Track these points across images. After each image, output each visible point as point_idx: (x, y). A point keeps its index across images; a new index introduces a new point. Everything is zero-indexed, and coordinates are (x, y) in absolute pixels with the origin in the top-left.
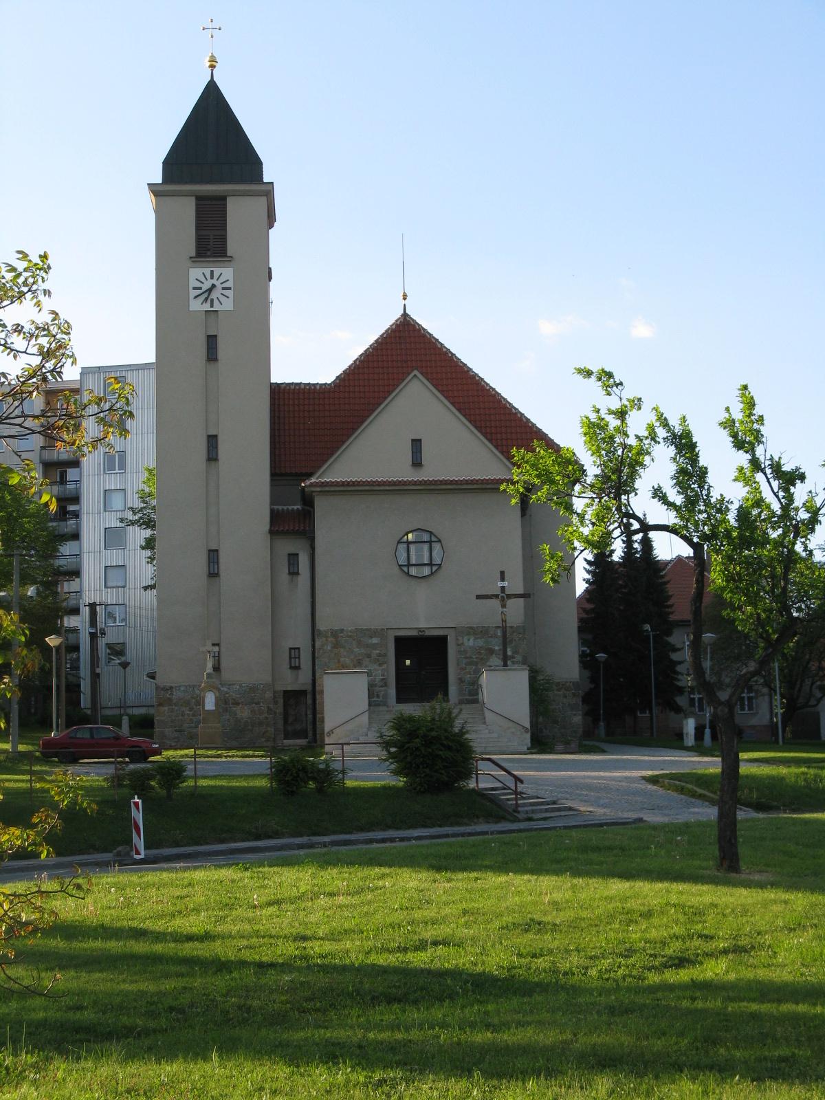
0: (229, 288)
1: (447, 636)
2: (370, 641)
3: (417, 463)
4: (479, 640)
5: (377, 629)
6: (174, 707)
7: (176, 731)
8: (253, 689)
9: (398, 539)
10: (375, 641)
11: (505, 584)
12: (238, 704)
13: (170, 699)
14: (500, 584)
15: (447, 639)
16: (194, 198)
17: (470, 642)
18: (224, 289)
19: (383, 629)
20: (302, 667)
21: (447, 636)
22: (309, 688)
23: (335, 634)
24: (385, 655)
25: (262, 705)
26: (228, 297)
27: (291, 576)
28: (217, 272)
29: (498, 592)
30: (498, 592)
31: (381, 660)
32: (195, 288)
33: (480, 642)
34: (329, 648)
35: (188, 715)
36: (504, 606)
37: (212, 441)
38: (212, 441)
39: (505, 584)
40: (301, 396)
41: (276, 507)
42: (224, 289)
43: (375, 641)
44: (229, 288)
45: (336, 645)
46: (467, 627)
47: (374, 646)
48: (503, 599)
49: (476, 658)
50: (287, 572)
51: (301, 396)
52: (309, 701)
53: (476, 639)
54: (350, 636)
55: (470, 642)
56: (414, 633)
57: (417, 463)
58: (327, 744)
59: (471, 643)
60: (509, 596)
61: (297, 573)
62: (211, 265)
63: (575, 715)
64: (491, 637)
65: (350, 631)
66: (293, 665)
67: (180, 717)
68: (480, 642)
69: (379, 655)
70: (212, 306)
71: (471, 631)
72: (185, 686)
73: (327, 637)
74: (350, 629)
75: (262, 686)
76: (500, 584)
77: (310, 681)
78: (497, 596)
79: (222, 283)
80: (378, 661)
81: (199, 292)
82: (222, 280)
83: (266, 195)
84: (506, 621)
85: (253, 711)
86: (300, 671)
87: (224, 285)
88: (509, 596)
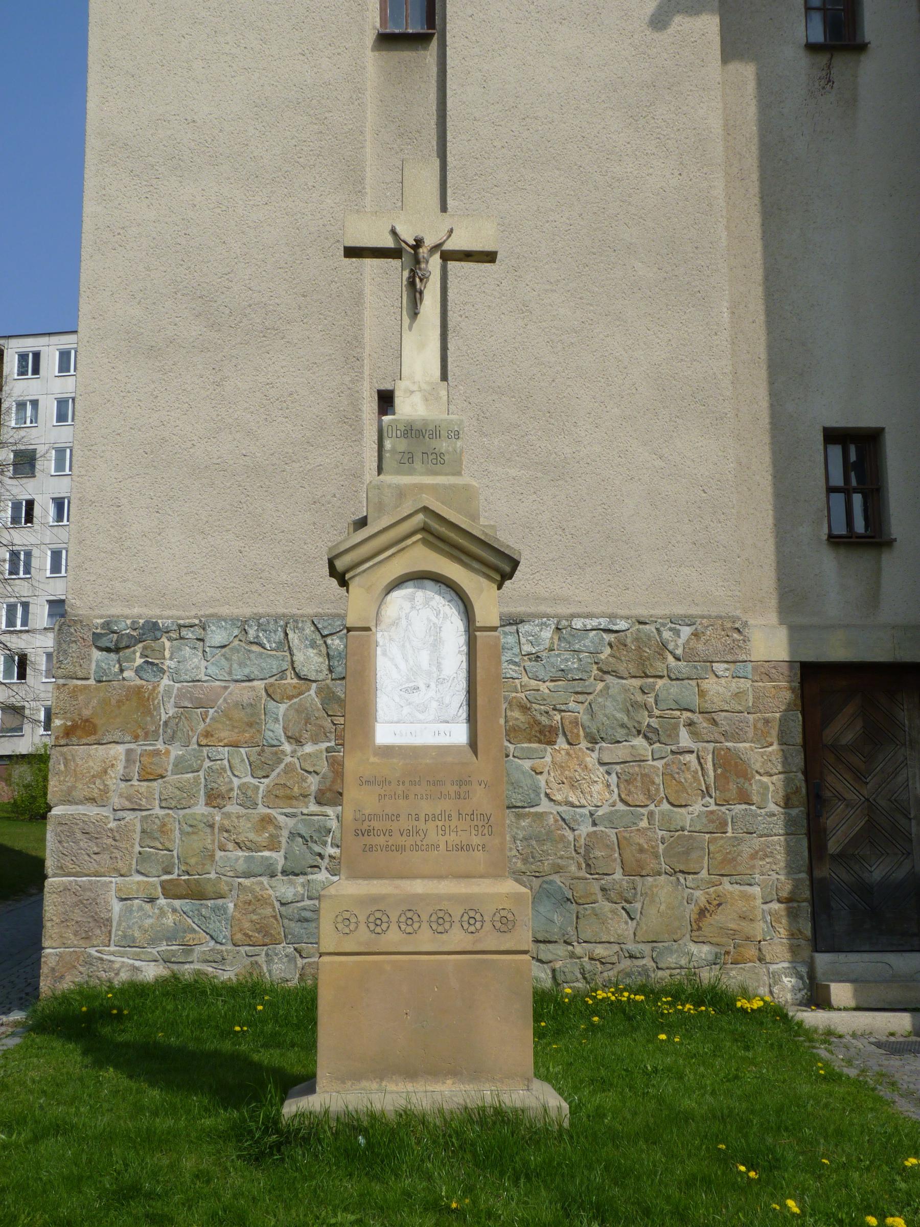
7: (170, 890)
27: (823, 59)
66: (840, 529)
67: (200, 809)
72: (233, 620)
75: (686, 631)
86: (888, 559)
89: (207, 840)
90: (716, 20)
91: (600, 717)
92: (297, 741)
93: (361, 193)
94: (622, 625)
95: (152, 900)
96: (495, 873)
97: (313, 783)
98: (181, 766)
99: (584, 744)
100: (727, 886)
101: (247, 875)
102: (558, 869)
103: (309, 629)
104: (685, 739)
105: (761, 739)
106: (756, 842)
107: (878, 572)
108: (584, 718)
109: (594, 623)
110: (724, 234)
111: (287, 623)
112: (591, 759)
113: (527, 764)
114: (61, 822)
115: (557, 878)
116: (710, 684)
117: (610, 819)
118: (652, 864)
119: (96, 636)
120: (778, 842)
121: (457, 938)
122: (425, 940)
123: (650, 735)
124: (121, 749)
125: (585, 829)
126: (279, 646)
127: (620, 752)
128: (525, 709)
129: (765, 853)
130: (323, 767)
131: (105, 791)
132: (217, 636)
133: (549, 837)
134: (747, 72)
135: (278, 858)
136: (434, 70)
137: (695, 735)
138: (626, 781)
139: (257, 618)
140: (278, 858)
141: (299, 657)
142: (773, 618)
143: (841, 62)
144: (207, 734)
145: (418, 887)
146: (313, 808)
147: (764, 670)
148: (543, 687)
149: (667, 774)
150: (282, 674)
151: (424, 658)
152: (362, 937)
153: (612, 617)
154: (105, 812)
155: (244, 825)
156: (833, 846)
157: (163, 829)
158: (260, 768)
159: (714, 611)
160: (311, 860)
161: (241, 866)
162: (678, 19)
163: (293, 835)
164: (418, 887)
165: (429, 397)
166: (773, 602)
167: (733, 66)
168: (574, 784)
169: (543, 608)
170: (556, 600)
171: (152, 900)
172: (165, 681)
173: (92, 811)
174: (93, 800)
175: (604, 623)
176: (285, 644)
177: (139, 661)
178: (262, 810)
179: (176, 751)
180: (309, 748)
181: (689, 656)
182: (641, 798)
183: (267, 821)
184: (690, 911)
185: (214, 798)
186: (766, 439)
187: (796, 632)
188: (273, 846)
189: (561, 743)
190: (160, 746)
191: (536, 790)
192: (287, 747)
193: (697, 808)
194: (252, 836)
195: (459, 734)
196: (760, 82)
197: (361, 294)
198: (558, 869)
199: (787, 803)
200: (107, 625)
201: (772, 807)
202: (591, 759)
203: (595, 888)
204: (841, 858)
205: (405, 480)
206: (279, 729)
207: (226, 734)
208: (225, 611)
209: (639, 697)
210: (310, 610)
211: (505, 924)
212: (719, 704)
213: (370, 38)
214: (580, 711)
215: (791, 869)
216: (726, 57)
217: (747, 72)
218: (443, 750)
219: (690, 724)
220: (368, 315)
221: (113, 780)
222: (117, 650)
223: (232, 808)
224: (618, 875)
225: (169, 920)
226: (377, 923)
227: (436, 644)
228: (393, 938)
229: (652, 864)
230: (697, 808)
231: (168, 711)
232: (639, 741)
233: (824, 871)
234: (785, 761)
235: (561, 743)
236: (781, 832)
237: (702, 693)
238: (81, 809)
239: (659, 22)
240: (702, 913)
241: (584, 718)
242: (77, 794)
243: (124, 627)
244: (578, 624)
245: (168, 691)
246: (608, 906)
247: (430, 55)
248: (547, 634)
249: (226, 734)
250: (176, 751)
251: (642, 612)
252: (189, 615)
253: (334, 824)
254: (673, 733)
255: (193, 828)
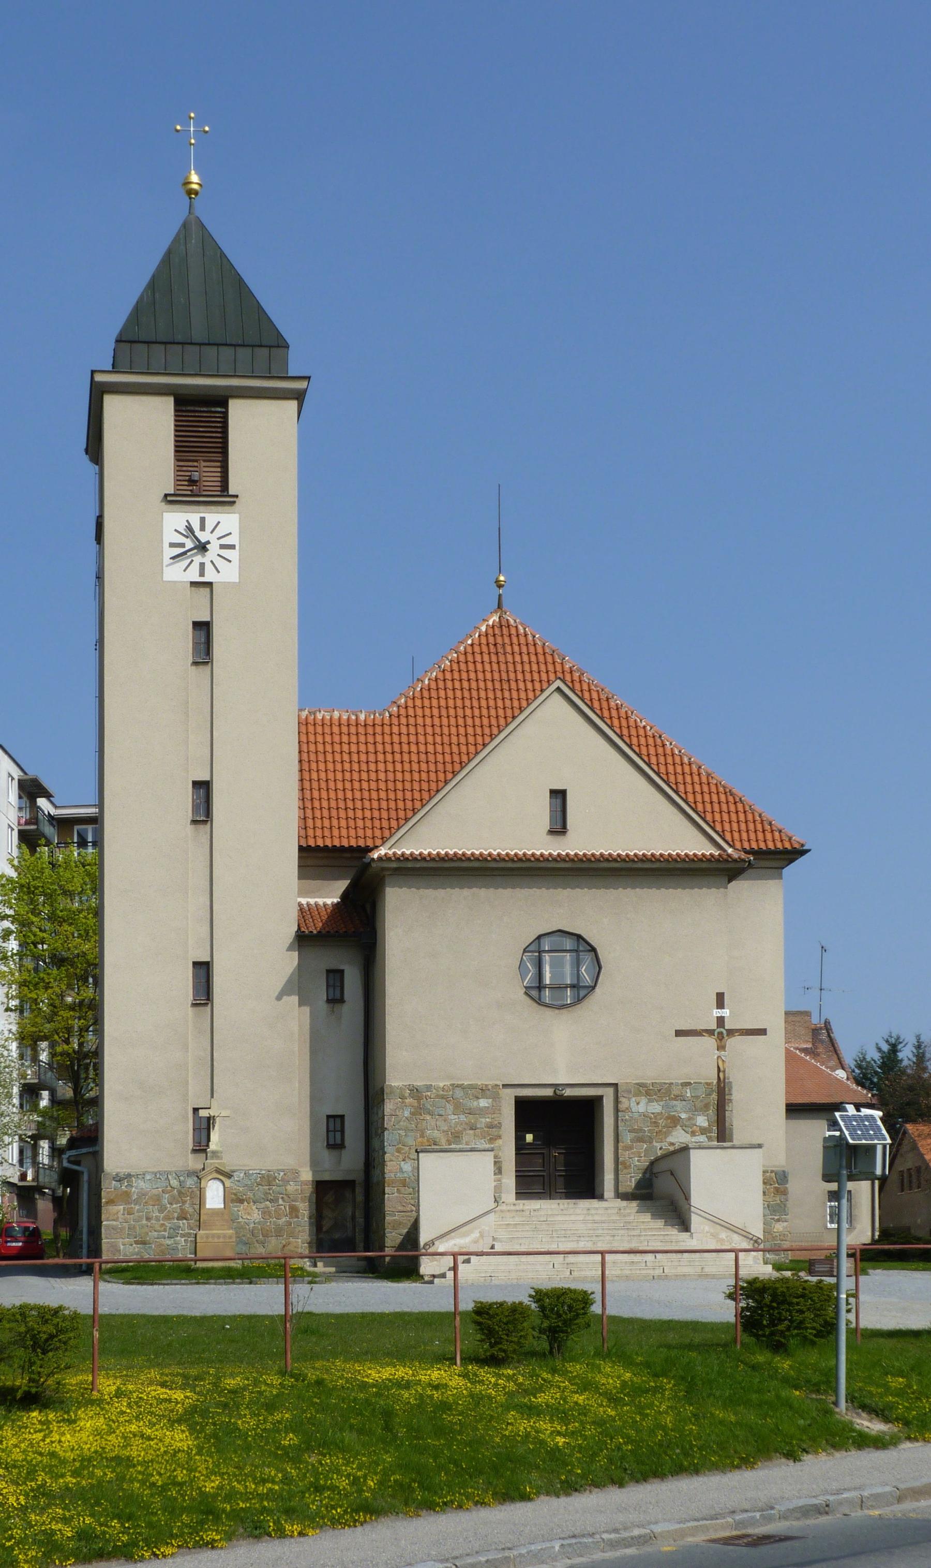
0: (232, 547)
1: (603, 1096)
2: (475, 1103)
3: (559, 828)
4: (655, 1103)
5: (486, 1085)
6: (133, 1206)
7: (136, 1242)
8: (268, 1179)
9: (524, 947)
10: (483, 1103)
11: (726, 1013)
12: (241, 1201)
13: (127, 1195)
14: (717, 1013)
15: (602, 1100)
16: (171, 400)
17: (640, 1106)
18: (223, 547)
19: (497, 1085)
20: (347, 1143)
21: (603, 1096)
22: (359, 1177)
23: (415, 1092)
24: (499, 1126)
25: (281, 1202)
26: (230, 561)
27: (331, 1005)
28: (212, 518)
29: (713, 1026)
30: (713, 1026)
31: (492, 1132)
32: (172, 545)
33: (656, 1108)
34: (407, 1114)
35: (158, 1219)
36: (721, 1048)
37: (203, 788)
38: (203, 788)
39: (726, 1013)
40: (336, 729)
41: (304, 901)
42: (223, 547)
43: (483, 1103)
44: (232, 547)
45: (419, 1111)
46: (637, 1084)
47: (482, 1112)
48: (721, 1037)
49: (649, 1131)
50: (325, 998)
51: (336, 729)
52: (360, 1198)
53: (650, 1101)
54: (443, 1097)
55: (640, 1106)
56: (549, 1092)
57: (559, 828)
58: (95, 1287)
59: (642, 1108)
60: (731, 1033)
61: (341, 1000)
62: (202, 508)
63: (778, 1220)
64: (675, 1099)
65: (443, 1090)
66: (332, 1142)
67: (144, 1222)
68: (656, 1108)
69: (490, 1126)
70: (202, 574)
71: (647, 1091)
72: (153, 1173)
73: (403, 1097)
74: (441, 1085)
75: (282, 1174)
76: (717, 1013)
77: (360, 1165)
78: (710, 1032)
79: (219, 539)
80: (489, 1135)
81: (181, 550)
82: (219, 532)
83: (297, 399)
84: (724, 1071)
85: (265, 1213)
86: (343, 1151)
87: (223, 541)
88: (731, 1033)
89: (146, 1230)
90: (297, 997)
91: (257, 1197)
92: (171, 1204)
93: (187, 1052)
94: (264, 1172)
95: (132, 1245)
96: (229, 1229)
97: (176, 1215)
98: (138, 1211)
99: (252, 1204)
100: (291, 1239)
101: (158, 1238)
102: (244, 1236)
103: (174, 1175)
104: (281, 1202)
105: (303, 1200)
106: (300, 1229)
107: (341, 1155)
108: (252, 1197)
109: (255, 1172)
110: (297, 1061)
111: (168, 1173)
112: (254, 1207)
113: (236, 1209)
114: (106, 1225)
115: (244, 1238)
116: (288, 1187)
117: (259, 1223)
118: (270, 1234)
119: (114, 1178)
120: (307, 1228)
121: (221, 1240)
122: (216, 1240)
123: (271, 1201)
124: (122, 1207)
125: (252, 1225)
126: (166, 1179)
127: (262, 1206)
128: (235, 1194)
129: (303, 1231)
130: (179, 1211)
131: (118, 1218)
132: (148, 1177)
133: (242, 1228)
134: (307, 1010)
135: (166, 1234)
136: (209, 1013)
137: (284, 1201)
138: (264, 1213)
139: (159, 1172)
140: (166, 1234)
141: (171, 1182)
142: (308, 1169)
143: (337, 1006)
144: (146, 1203)
145: (215, 1232)
146: (176, 1221)
147: (305, 1183)
148: (241, 1189)
149: (275, 1211)
150: (167, 1187)
151: (215, 1193)
152: (205, 1240)
153: (261, 1170)
154: (118, 1223)
155: (156, 1226)
156: (324, 1229)
157: (134, 1227)
158: (161, 1211)
159: (290, 1168)
160: (175, 1234)
161: (156, 1236)
162: (285, 997)
163: (170, 1228)
164: (215, 1232)
165: (217, 1145)
166: (309, 1164)
167: (302, 1008)
168: (249, 1214)
169: (241, 1168)
170: (245, 1166)
171: (132, 1245)
172: (134, 1189)
173: (114, 1223)
174: (114, 1220)
175: (258, 1171)
176: (167, 1178)
177: (126, 1184)
178: (162, 1222)
179: (137, 1207)
180: (174, 1206)
181: (283, 1180)
182: (268, 1217)
183: (163, 1225)
184: (281, 1246)
185: (148, 1219)
186: (308, 1119)
187: (314, 1172)
188: (165, 1230)
189: (246, 1203)
190: (133, 1206)
191: (238, 1216)
192: (168, 1206)
193: (284, 1219)
194: (159, 1228)
195: (222, 1206)
196: (311, 1012)
197: (188, 1081)
198: (244, 1236)
199: (310, 1218)
200: (117, 1174)
201: (306, 1219)
202: (254, 1207)
203: (255, 1240)
204: (327, 1232)
205: (212, 1161)
206: (166, 1201)
207: (151, 1203)
208: (150, 1170)
209: (268, 1191)
210: (174, 1169)
211: (230, 1237)
212: (291, 1193)
213: (190, 1003)
214: (250, 1194)
215: (310, 1235)
216: (300, 1005)
217: (307, 1010)
218: (219, 1209)
219: (282, 1198)
220: (190, 1088)
221: (120, 1215)
222: (120, 1181)
223: (153, 1222)
224: (261, 1237)
225: (136, 1250)
226: (207, 1237)
227: (217, 1190)
228: (210, 1240)
229: (270, 1234)
230: (284, 1219)
231: (135, 1197)
232: (268, 1203)
233: (321, 1236)
234: (310, 1207)
235: (246, 1203)
236: (743, 1273)
237: (286, 1190)
238: (111, 1222)
239: (279, 998)
240: (284, 1246)
241: (252, 1197)
242: (110, 1219)
243: (121, 1175)
244: (251, 1172)
245: (134, 1192)
246: (258, 1245)
247: (208, 1008)
248: (242, 1175)
249: (151, 1203)
250: (137, 1207)
251: (269, 1168)
252: (139, 1171)
253: (181, 1225)
254: (277, 1200)
255: (142, 1227)
